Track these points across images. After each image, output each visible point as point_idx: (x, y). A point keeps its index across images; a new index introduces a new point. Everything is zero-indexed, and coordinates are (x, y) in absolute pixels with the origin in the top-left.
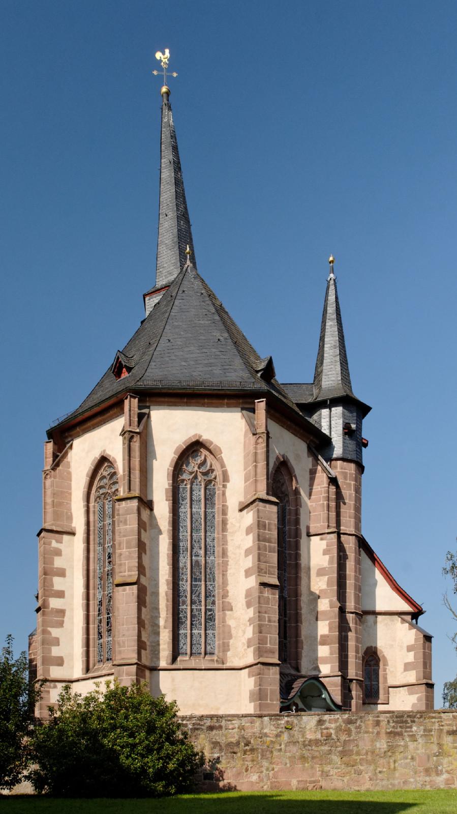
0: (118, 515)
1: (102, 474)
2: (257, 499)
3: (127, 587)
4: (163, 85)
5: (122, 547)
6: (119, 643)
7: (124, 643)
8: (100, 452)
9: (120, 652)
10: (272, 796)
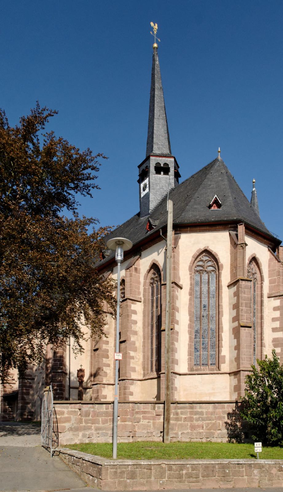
0: (241, 288)
1: (200, 258)
2: (174, 282)
3: (247, 328)
4: (154, 43)
5: (243, 305)
6: (242, 359)
7: (244, 358)
8: (204, 247)
9: (242, 364)
10: (5, 435)
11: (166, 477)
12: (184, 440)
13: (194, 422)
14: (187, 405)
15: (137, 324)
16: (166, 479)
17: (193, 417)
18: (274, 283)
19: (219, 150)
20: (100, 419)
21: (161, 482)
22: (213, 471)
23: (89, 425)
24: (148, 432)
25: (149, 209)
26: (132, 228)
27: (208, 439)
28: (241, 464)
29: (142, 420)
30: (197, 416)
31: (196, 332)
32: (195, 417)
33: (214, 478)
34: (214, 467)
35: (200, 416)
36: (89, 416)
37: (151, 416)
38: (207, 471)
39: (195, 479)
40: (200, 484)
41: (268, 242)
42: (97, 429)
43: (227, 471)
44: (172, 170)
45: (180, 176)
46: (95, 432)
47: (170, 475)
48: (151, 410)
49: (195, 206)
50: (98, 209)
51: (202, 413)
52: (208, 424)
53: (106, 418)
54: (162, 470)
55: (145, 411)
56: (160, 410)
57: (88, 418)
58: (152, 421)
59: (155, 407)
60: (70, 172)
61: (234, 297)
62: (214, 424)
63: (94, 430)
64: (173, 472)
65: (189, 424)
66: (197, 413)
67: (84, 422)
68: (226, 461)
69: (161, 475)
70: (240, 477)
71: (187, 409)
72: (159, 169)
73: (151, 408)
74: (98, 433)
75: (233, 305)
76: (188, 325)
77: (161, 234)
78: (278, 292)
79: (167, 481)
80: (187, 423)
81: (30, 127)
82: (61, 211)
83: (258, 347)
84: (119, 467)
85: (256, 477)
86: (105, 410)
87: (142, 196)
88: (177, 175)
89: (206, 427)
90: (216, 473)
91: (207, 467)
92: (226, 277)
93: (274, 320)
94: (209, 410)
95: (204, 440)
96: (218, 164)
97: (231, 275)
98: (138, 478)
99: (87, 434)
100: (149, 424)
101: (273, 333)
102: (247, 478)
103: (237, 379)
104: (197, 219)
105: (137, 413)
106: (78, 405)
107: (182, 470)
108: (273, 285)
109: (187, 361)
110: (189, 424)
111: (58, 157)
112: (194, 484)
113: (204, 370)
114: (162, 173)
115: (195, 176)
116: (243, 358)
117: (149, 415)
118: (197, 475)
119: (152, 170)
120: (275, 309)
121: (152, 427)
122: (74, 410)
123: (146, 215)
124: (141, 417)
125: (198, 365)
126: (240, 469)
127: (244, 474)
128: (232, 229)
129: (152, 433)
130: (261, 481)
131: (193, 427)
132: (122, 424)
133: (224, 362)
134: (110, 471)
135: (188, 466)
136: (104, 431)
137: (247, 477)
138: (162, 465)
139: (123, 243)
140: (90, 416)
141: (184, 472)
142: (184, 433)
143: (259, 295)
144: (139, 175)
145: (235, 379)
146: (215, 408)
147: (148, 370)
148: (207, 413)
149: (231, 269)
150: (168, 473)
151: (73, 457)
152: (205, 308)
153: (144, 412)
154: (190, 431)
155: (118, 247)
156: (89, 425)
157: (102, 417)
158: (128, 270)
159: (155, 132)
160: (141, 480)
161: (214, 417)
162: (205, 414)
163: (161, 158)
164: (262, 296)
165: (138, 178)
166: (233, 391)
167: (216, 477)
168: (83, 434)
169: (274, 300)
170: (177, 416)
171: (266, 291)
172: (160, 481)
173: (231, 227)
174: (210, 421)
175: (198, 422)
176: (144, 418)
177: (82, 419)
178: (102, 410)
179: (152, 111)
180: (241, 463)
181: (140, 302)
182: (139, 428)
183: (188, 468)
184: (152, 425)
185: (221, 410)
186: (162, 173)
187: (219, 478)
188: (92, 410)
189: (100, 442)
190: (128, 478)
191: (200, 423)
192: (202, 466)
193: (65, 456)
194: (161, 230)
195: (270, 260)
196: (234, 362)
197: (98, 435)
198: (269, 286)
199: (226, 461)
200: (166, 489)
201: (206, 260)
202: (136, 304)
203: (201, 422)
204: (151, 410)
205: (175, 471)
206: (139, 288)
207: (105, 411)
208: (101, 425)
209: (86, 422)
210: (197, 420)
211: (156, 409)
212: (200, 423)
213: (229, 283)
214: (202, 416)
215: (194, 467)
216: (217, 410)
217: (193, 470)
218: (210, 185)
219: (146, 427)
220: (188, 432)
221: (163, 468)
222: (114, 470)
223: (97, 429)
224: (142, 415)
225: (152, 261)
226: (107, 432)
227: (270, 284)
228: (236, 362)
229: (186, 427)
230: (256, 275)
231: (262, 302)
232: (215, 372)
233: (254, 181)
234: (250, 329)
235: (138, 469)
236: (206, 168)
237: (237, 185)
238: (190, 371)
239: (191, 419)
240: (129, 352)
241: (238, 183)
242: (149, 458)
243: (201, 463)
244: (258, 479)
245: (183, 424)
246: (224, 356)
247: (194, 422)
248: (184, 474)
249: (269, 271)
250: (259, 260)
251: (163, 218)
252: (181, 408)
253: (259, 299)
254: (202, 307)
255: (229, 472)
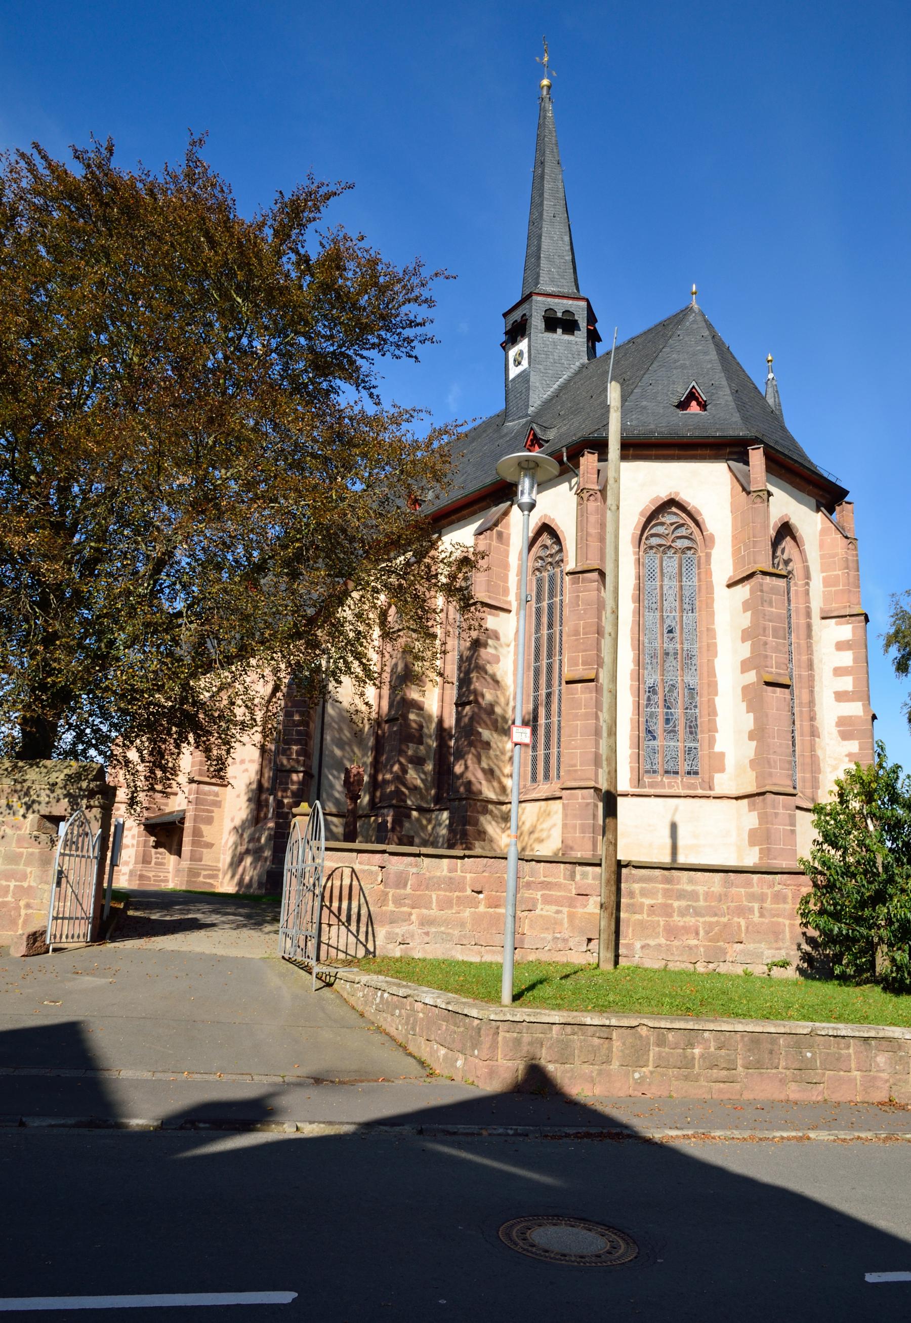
3: (778, 689)
7: (775, 762)
11: (651, 1063)
12: (648, 964)
13: (676, 918)
14: (657, 872)
15: (501, 663)
16: (651, 1068)
17: (672, 904)
18: (834, 586)
19: (694, 290)
20: (434, 897)
21: (637, 1075)
22: (771, 1052)
23: (405, 909)
24: (555, 939)
25: (527, 406)
26: (485, 445)
27: (711, 966)
28: (843, 1037)
29: (539, 906)
30: (683, 903)
31: (649, 692)
32: (676, 904)
33: (774, 1071)
34: (774, 1042)
35: (689, 903)
36: (405, 886)
37: (561, 896)
38: (756, 1051)
39: (725, 1073)
40: (737, 1086)
41: (816, 490)
42: (425, 922)
43: (809, 1055)
44: (583, 324)
45: (599, 340)
46: (420, 931)
47: (660, 1056)
48: (565, 879)
49: (644, 403)
50: (419, 394)
51: (694, 896)
52: (711, 924)
53: (447, 894)
54: (639, 1042)
55: (549, 883)
56: (586, 881)
57: (402, 891)
58: (565, 910)
59: (574, 872)
60: (360, 312)
61: (744, 612)
62: (725, 925)
63: (416, 923)
64: (667, 1050)
65: (662, 923)
66: (681, 895)
67: (390, 902)
68: (804, 1027)
69: (636, 1058)
70: (842, 1073)
71: (656, 882)
72: (552, 323)
73: (564, 874)
74: (427, 934)
75: (743, 631)
76: (630, 672)
77: (565, 459)
78: (845, 607)
79: (651, 1073)
80: (657, 919)
81: (295, 213)
82: (341, 393)
83: (802, 735)
84: (528, 1028)
85: (882, 1075)
86: (445, 873)
87: (512, 376)
88: (593, 337)
89: (707, 933)
90: (779, 1059)
91: (755, 1039)
92: (722, 563)
93: (839, 672)
94: (712, 889)
95: (701, 968)
96: (691, 318)
97: (734, 561)
98: (577, 1062)
99: (397, 934)
100: (559, 916)
101: (837, 703)
102: (862, 1077)
103: (756, 813)
104: (652, 432)
105: (528, 885)
106: (378, 856)
107: (692, 1045)
108: (833, 589)
109: (629, 760)
110: (662, 923)
111: (350, 278)
112: (722, 1085)
113: (670, 786)
114: (559, 331)
115: (639, 340)
116: (772, 761)
117: (559, 894)
118: (729, 1061)
119: (537, 322)
120: (841, 646)
121: (566, 925)
122: (367, 867)
123: (519, 418)
124: (539, 897)
125: (654, 772)
126: (842, 1052)
127: (853, 1066)
128: (735, 457)
129: (565, 940)
130: (895, 1084)
131: (672, 932)
132: (488, 912)
133: (722, 770)
134: (505, 1037)
135: (706, 1034)
136: (443, 929)
137: (859, 1073)
138: (639, 1029)
139: (537, 465)
140: (409, 886)
141: (697, 1051)
142: (648, 945)
143: (802, 612)
144: (506, 333)
145: (752, 813)
146: (727, 884)
147: (525, 780)
148: (707, 895)
149: (733, 546)
150: (654, 1051)
151: (379, 993)
152: (671, 635)
153: (545, 885)
154: (663, 941)
155: (525, 475)
156: (405, 909)
157: (439, 890)
158: (482, 537)
159: (544, 246)
160: (586, 1065)
161: (725, 907)
162: (701, 897)
163: (557, 300)
164: (808, 615)
165: (503, 338)
166: (747, 842)
167: (781, 1070)
168: (388, 933)
169: (837, 624)
170: (632, 901)
171: (817, 604)
172: (634, 1071)
173: (731, 453)
174: (716, 919)
175: (684, 919)
176: (547, 900)
177: (387, 894)
178: (438, 874)
179: (537, 204)
180: (843, 1033)
181: (509, 611)
182: (531, 927)
183: (708, 1040)
184: (566, 920)
185: (743, 890)
186: (559, 331)
187: (788, 1072)
188: (414, 870)
189: (429, 956)
190: (549, 1059)
191: (690, 920)
192: (742, 1036)
193: (351, 987)
194: (564, 450)
195: (823, 532)
196: (749, 769)
197: (427, 939)
198: (824, 592)
199: (804, 1027)
200: (649, 1095)
201: (672, 524)
202: (498, 616)
203: (693, 920)
204: (565, 879)
205: (673, 1046)
206: (505, 579)
207: (445, 877)
208: (434, 912)
209: (398, 901)
210: (683, 913)
211: (578, 877)
212: (690, 920)
213: (730, 579)
214: (694, 904)
215: (724, 1040)
216: (734, 890)
217: (720, 1048)
218: (676, 361)
219: (551, 924)
220: (660, 945)
221: (641, 1036)
222: (515, 1035)
223: (425, 922)
224: (540, 893)
225: (540, 520)
226: (450, 931)
227: (825, 586)
228: (753, 770)
229: (655, 928)
230: (791, 564)
231: (809, 627)
232: (700, 792)
233: (770, 358)
234: (787, 690)
235: (575, 1037)
236: (663, 325)
237: (738, 363)
238: (634, 787)
239: (667, 911)
240: (480, 730)
241: (739, 360)
242: (602, 1009)
243: (740, 1028)
244: (887, 1081)
245: (648, 921)
246: (722, 755)
247: (676, 918)
248: (697, 1057)
249: (822, 557)
250: (798, 531)
251: (565, 425)
252: (642, 880)
253: (803, 621)
254: (665, 631)
255: (813, 1058)
